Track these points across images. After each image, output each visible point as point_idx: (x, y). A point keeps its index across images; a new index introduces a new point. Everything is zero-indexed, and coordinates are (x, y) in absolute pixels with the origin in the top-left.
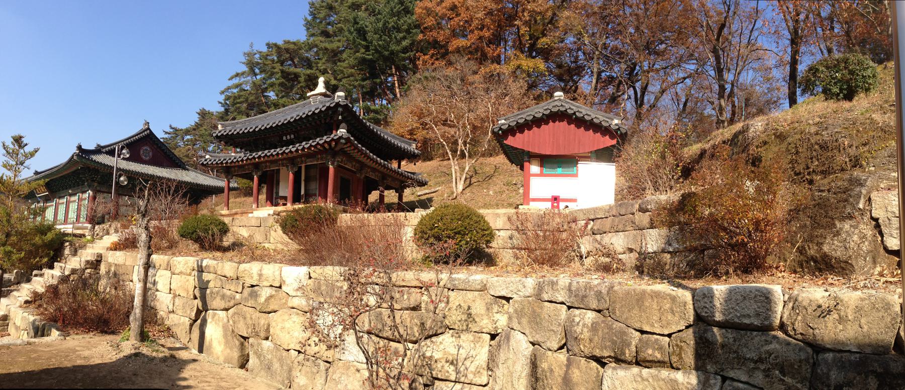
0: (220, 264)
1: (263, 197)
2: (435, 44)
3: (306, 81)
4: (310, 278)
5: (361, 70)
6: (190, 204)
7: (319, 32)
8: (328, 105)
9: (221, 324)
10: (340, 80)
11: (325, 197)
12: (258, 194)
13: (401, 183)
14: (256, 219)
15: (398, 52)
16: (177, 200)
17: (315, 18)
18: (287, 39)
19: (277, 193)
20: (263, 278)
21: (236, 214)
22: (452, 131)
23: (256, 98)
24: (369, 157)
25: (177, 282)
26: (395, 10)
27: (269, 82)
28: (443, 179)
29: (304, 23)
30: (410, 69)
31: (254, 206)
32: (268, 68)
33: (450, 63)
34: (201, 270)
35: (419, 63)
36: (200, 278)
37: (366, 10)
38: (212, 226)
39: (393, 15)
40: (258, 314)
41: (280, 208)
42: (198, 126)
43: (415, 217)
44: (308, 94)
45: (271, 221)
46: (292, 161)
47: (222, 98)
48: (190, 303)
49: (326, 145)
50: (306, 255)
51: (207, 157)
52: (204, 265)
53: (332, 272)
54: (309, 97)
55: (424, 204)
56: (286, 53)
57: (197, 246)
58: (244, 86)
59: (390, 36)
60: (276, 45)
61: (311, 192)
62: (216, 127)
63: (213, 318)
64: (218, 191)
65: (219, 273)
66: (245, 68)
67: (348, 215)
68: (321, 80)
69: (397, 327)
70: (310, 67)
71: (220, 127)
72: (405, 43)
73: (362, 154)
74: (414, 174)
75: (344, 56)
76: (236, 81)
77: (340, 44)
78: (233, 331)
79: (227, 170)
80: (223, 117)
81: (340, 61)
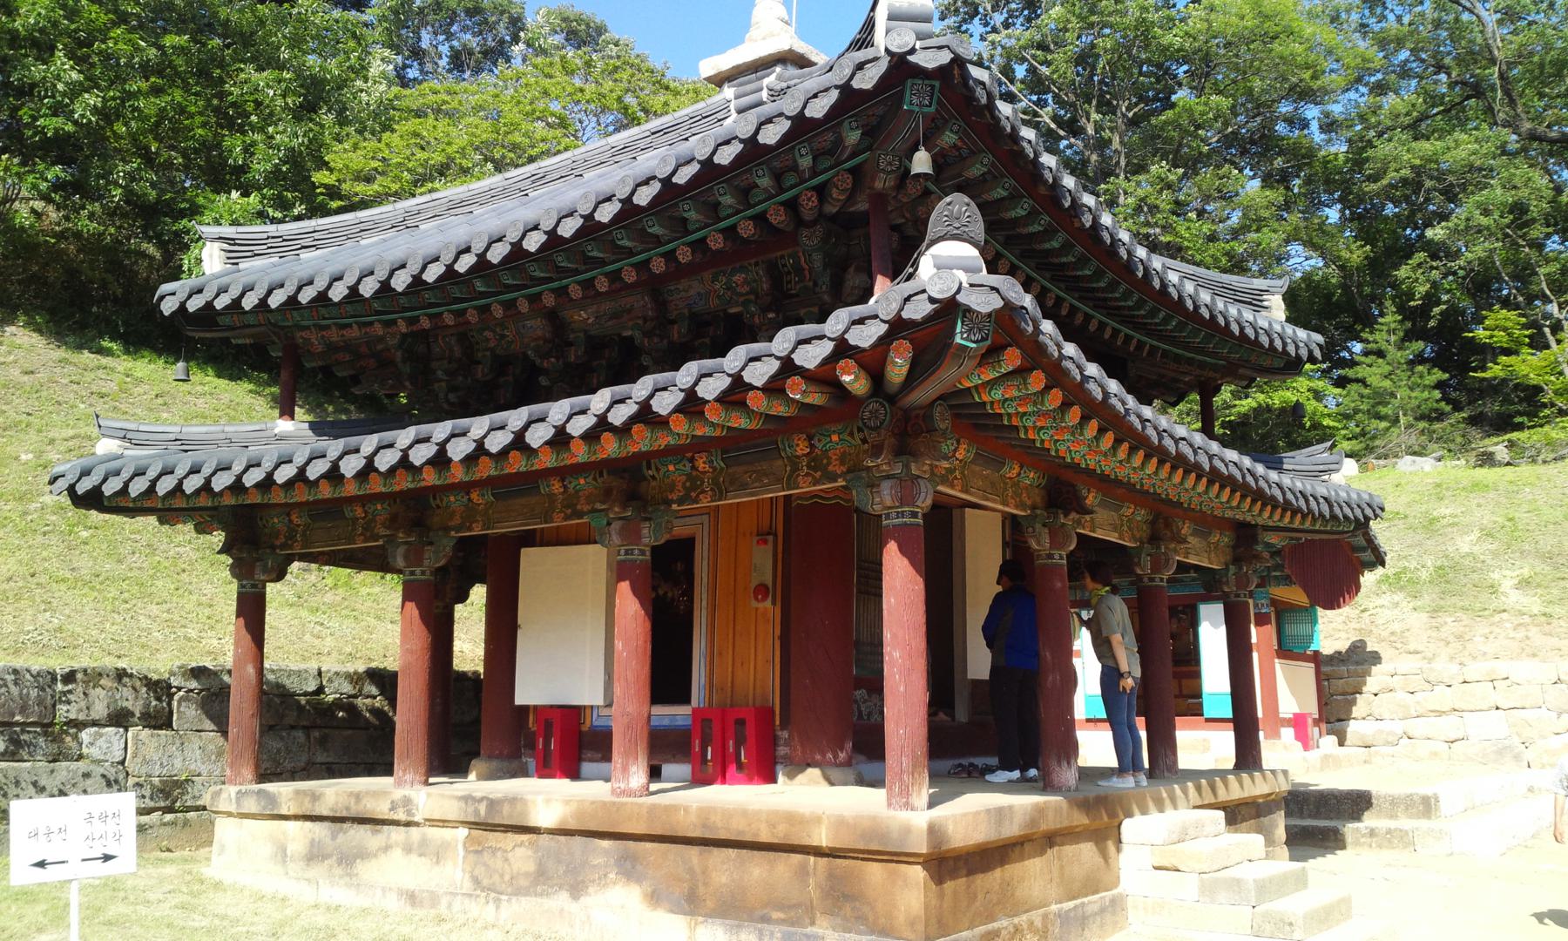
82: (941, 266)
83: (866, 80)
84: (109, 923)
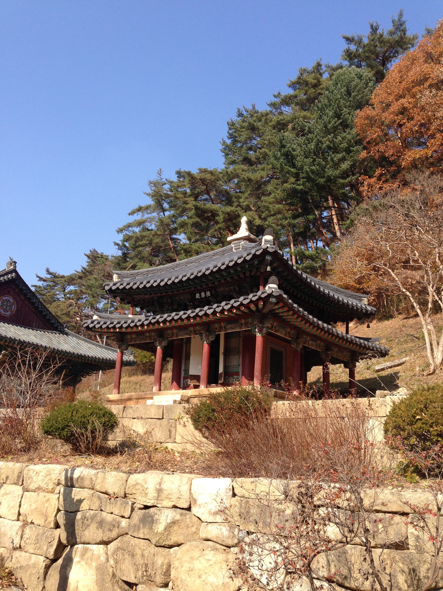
0: (100, 475)
1: (168, 375)
2: (383, 161)
3: (225, 221)
4: (234, 495)
5: (290, 204)
6: (65, 385)
7: (241, 158)
8: (253, 252)
9: (94, 564)
10: (265, 219)
11: (251, 378)
12: (162, 371)
13: (352, 353)
14: (157, 408)
15: (336, 177)
16: (45, 378)
17: (235, 141)
18: (203, 167)
19: (187, 371)
20: (163, 495)
21: (130, 399)
22: (417, 275)
23: (163, 241)
24: (307, 321)
25: (31, 503)
26: (329, 126)
27: (180, 220)
28: (410, 345)
29: (221, 147)
30: (352, 198)
31: (155, 389)
32: (179, 203)
33: (405, 184)
34: (70, 484)
35: (364, 189)
36: (67, 496)
37: (294, 129)
38: (93, 418)
39: (327, 132)
40: (153, 549)
41: (190, 392)
42: (86, 273)
43: (383, 404)
44: (229, 239)
45: (179, 410)
46: (207, 327)
47: (119, 238)
48: (48, 534)
49: (252, 307)
50: (227, 461)
51: (95, 317)
52: (75, 476)
53: (267, 487)
54: (230, 243)
55: (390, 383)
56: (201, 184)
57: (67, 447)
58: (148, 225)
59: (325, 159)
60: (189, 174)
61: (232, 370)
62: (110, 277)
63: (83, 555)
64: (107, 365)
65: (98, 487)
66: (150, 202)
67: (286, 402)
68: (244, 219)
69: (377, 576)
70: (229, 202)
71: (115, 278)
72: (345, 166)
73: (299, 316)
74: (368, 339)
75: (270, 188)
76: (138, 217)
77: (264, 174)
78: (114, 575)
79: (121, 337)
80: (121, 263)
81: (264, 195)
82: (269, 287)
83: (258, 253)
84: (170, 431)
